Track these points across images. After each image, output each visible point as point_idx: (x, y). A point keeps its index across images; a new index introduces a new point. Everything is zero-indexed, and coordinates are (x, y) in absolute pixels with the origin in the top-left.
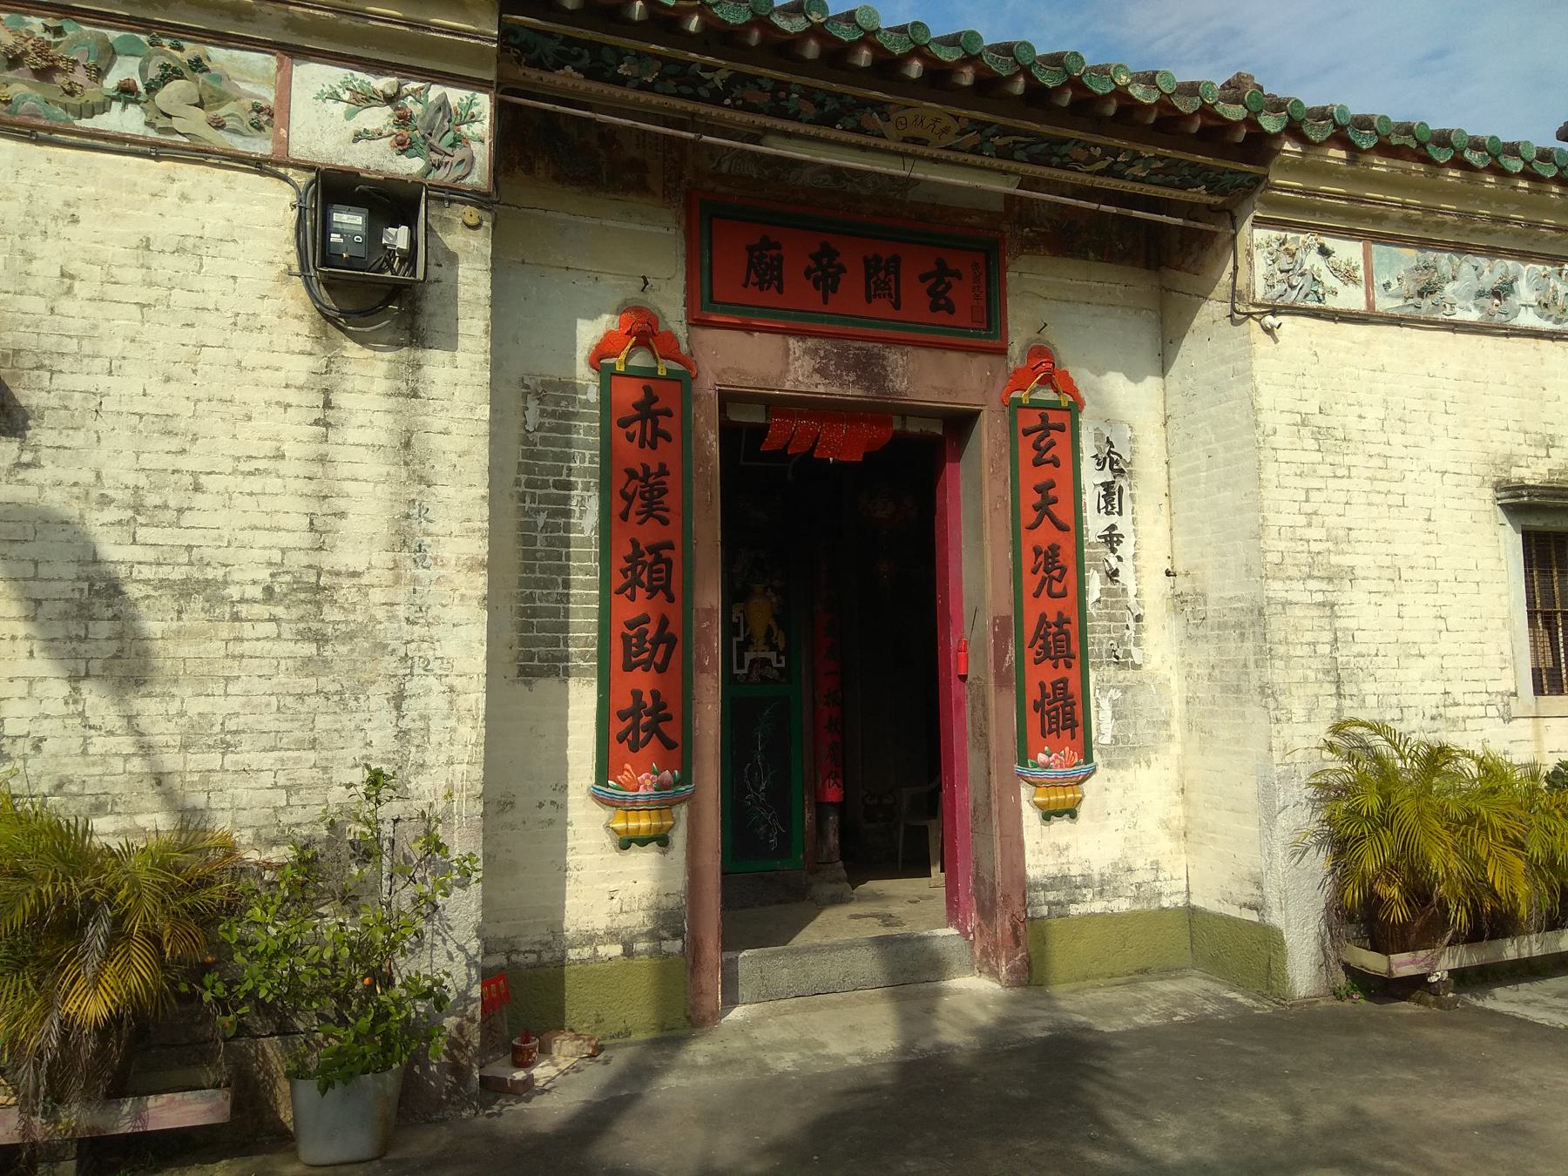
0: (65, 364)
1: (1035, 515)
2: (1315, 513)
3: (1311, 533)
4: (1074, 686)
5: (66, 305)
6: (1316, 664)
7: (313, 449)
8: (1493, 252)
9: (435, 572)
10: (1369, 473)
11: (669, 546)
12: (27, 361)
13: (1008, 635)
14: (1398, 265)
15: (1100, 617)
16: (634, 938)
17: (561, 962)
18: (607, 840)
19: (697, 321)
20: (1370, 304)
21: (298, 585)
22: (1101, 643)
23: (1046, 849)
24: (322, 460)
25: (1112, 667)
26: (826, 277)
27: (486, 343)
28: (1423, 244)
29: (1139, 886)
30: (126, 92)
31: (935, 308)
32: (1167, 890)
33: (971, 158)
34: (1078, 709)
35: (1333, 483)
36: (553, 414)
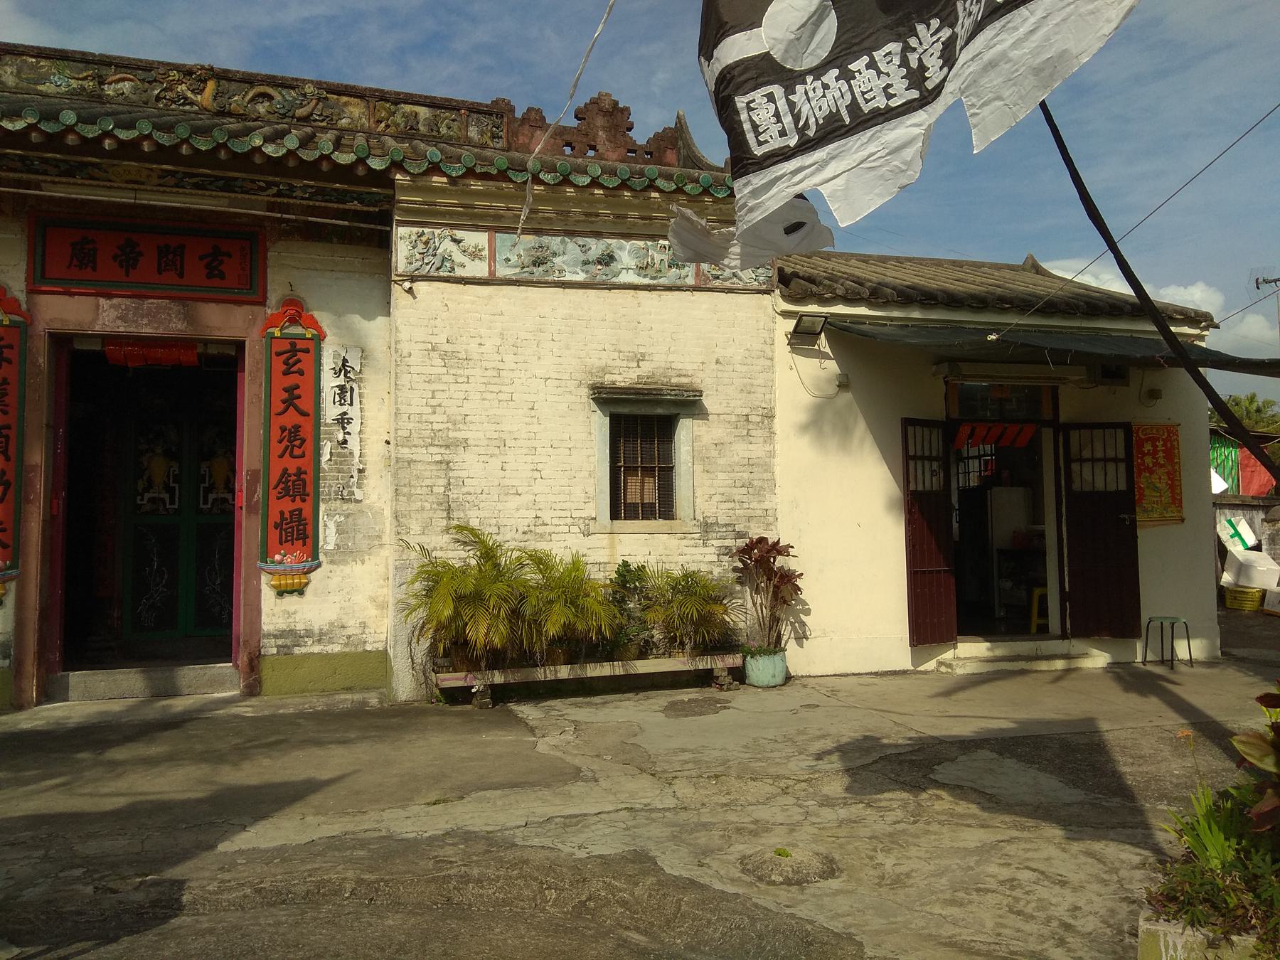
1: (283, 406)
8: (598, 235)
11: (9, 427)
14: (515, 250)
15: (331, 470)
19: (32, 291)
20: (492, 272)
22: (330, 486)
23: (274, 612)
28: (538, 232)
31: (209, 276)
32: (371, 640)
33: (174, 190)
34: (309, 528)
35: (453, 387)
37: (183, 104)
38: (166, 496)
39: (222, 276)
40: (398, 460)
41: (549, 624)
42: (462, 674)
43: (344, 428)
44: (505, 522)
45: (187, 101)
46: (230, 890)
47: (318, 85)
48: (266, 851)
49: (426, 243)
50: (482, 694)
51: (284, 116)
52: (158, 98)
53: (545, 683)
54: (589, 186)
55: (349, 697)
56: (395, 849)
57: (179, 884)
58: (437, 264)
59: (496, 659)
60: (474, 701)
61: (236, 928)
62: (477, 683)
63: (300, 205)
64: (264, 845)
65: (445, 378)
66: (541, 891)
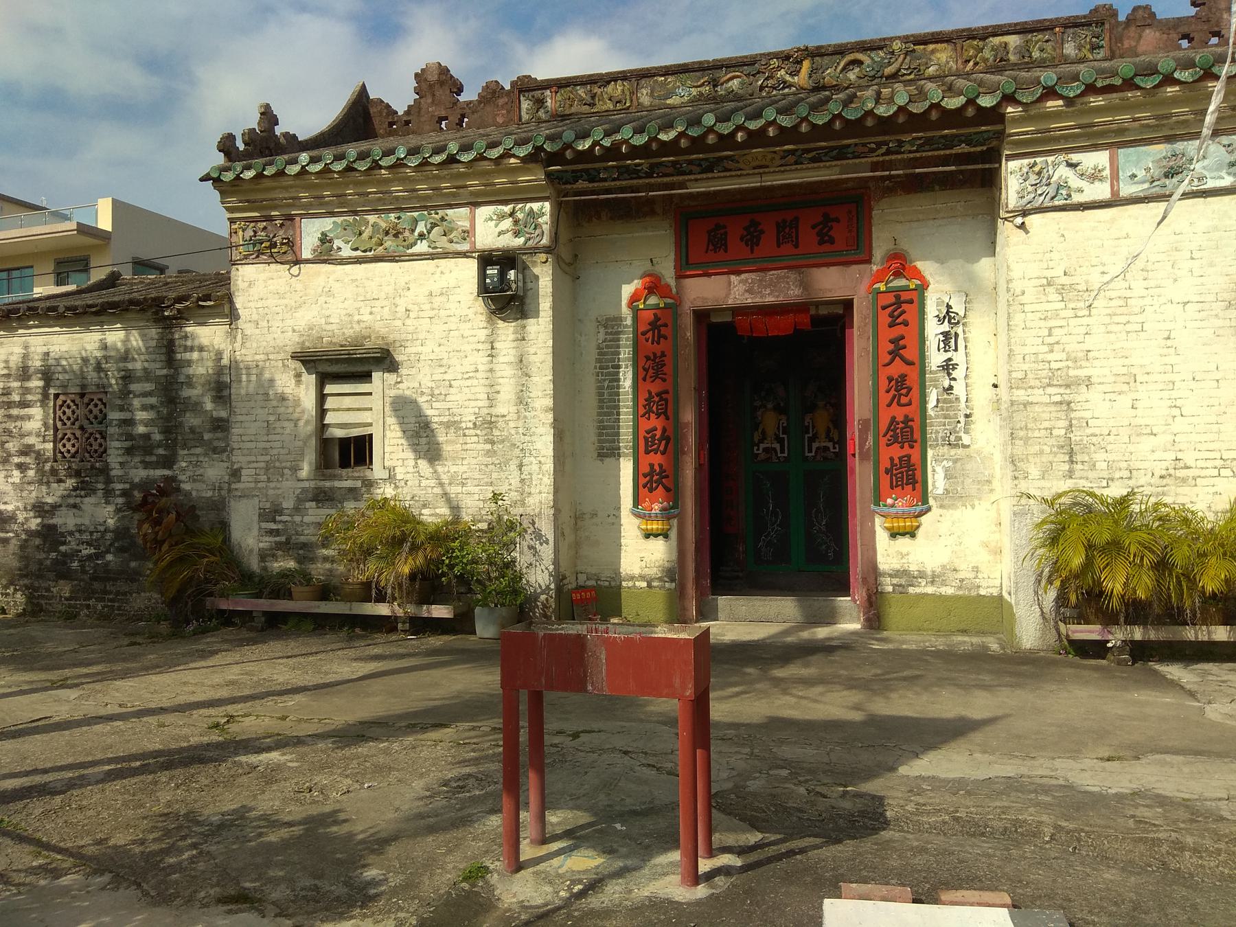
0: (408, 344)
2: (1057, 343)
3: (1050, 357)
5: (408, 322)
6: (1052, 441)
7: (487, 367)
9: (533, 413)
12: (398, 344)
13: (868, 430)
14: (1142, 162)
15: (937, 417)
16: (652, 580)
19: (680, 276)
21: (485, 422)
23: (890, 554)
24: (491, 370)
25: (946, 447)
28: (1170, 139)
29: (962, 580)
30: (422, 236)
32: (984, 584)
33: (794, 167)
35: (1073, 322)
36: (611, 333)
37: (783, 88)
38: (777, 446)
40: (1012, 403)
42: (1098, 627)
43: (949, 374)
44: (1138, 465)
47: (906, 39)
48: (944, 780)
49: (1039, 173)
50: (1121, 650)
51: (874, 77)
52: (762, 88)
54: (1082, 94)
55: (966, 639)
56: (1078, 802)
58: (1052, 194)
59: (1136, 611)
60: (1109, 655)
62: (1116, 637)
63: (903, 159)
65: (1063, 314)
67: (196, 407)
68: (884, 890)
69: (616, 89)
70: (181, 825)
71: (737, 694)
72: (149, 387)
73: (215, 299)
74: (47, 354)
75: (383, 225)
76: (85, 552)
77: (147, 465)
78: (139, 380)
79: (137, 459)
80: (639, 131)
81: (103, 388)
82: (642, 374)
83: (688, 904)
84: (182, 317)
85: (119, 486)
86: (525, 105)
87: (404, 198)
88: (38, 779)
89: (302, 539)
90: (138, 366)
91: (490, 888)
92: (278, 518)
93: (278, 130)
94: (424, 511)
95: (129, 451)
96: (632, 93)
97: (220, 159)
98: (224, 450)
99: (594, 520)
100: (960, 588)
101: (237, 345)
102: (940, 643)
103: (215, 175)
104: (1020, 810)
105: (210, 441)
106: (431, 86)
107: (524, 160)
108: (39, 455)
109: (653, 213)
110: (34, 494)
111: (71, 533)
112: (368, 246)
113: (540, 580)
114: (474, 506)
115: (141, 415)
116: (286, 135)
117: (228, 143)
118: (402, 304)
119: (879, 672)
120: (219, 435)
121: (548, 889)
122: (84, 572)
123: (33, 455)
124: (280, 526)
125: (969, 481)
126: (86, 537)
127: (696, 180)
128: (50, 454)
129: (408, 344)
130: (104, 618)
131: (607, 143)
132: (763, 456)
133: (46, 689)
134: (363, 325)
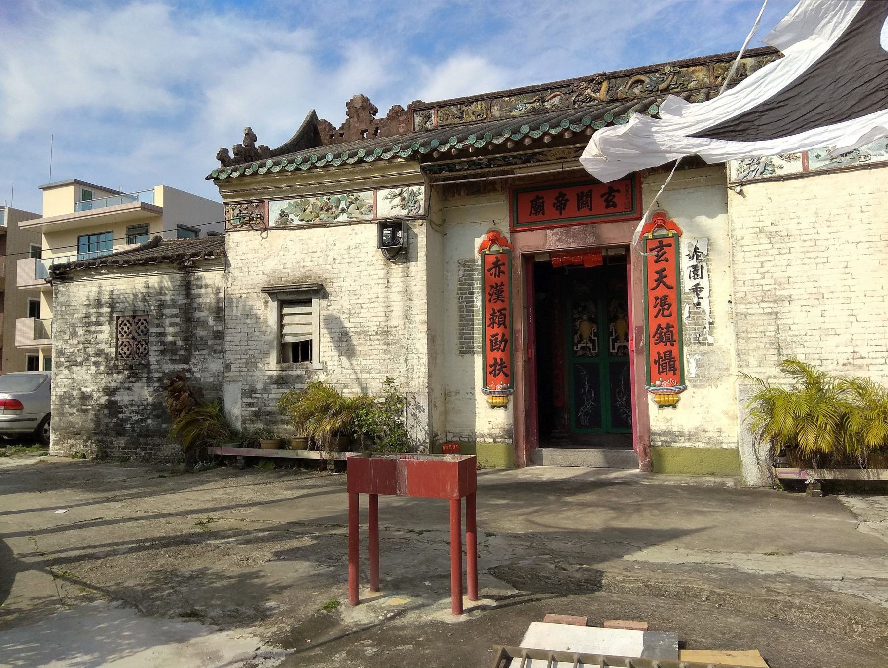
0: (335, 281)
1: (655, 284)
2: (768, 272)
3: (762, 282)
4: (675, 353)
5: (335, 266)
9: (414, 325)
10: (804, 249)
15: (690, 324)
16: (497, 437)
17: (475, 442)
18: (487, 405)
19: (512, 232)
24: (387, 297)
26: (561, 205)
27: (425, 258)
29: (710, 438)
30: (343, 210)
32: (726, 441)
35: (778, 257)
37: (589, 101)
38: (591, 346)
39: (615, 205)
41: (870, 436)
42: (797, 470)
43: (697, 295)
45: (592, 99)
46: (630, 582)
47: (674, 64)
48: (653, 564)
50: (814, 486)
52: (574, 102)
53: (869, 482)
55: (712, 479)
56: (737, 577)
57: (601, 573)
58: (761, 170)
59: (823, 460)
60: (807, 490)
61: (633, 604)
62: (811, 476)
64: (652, 561)
65: (771, 252)
66: (850, 624)
67: (203, 324)
68: (570, 618)
69: (477, 107)
70: (169, 577)
71: (536, 512)
72: (175, 311)
73: (214, 253)
74: (112, 291)
75: (319, 204)
76: (134, 418)
77: (173, 362)
78: (169, 307)
79: (168, 358)
80: (479, 138)
81: (146, 312)
82: (488, 297)
83: (453, 624)
84: (195, 266)
85: (156, 375)
86: (418, 120)
87: (332, 186)
88: (90, 551)
89: (268, 409)
90: (168, 298)
91: (339, 613)
92: (253, 395)
93: (257, 145)
94: (345, 390)
95: (162, 353)
96: (487, 109)
97: (218, 165)
98: (221, 352)
99: (458, 396)
100: (708, 443)
101: (229, 284)
102: (691, 481)
103: (215, 176)
104: (691, 582)
105: (212, 346)
106: (357, 110)
107: (407, 159)
108: (107, 355)
109: (494, 190)
110: (104, 381)
111: (126, 406)
112: (309, 218)
113: (419, 436)
114: (376, 388)
115: (170, 330)
116: (261, 147)
117: (223, 155)
118: (331, 254)
119: (640, 499)
120: (218, 342)
121: (373, 615)
122: (133, 430)
123: (104, 356)
124: (255, 401)
125: (713, 369)
126: (135, 408)
127: (520, 168)
128: (113, 355)
129: (335, 281)
130: (146, 460)
131: (459, 146)
132: (581, 353)
133: (103, 502)
134: (306, 269)
